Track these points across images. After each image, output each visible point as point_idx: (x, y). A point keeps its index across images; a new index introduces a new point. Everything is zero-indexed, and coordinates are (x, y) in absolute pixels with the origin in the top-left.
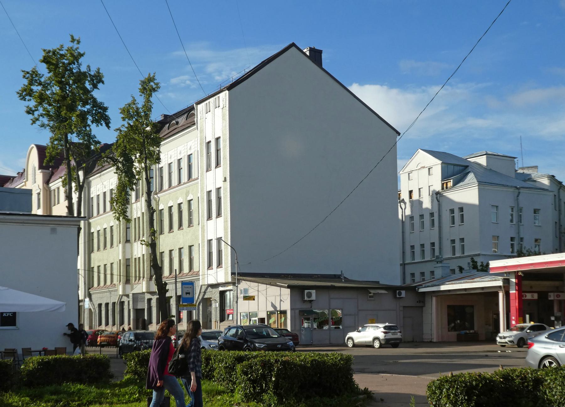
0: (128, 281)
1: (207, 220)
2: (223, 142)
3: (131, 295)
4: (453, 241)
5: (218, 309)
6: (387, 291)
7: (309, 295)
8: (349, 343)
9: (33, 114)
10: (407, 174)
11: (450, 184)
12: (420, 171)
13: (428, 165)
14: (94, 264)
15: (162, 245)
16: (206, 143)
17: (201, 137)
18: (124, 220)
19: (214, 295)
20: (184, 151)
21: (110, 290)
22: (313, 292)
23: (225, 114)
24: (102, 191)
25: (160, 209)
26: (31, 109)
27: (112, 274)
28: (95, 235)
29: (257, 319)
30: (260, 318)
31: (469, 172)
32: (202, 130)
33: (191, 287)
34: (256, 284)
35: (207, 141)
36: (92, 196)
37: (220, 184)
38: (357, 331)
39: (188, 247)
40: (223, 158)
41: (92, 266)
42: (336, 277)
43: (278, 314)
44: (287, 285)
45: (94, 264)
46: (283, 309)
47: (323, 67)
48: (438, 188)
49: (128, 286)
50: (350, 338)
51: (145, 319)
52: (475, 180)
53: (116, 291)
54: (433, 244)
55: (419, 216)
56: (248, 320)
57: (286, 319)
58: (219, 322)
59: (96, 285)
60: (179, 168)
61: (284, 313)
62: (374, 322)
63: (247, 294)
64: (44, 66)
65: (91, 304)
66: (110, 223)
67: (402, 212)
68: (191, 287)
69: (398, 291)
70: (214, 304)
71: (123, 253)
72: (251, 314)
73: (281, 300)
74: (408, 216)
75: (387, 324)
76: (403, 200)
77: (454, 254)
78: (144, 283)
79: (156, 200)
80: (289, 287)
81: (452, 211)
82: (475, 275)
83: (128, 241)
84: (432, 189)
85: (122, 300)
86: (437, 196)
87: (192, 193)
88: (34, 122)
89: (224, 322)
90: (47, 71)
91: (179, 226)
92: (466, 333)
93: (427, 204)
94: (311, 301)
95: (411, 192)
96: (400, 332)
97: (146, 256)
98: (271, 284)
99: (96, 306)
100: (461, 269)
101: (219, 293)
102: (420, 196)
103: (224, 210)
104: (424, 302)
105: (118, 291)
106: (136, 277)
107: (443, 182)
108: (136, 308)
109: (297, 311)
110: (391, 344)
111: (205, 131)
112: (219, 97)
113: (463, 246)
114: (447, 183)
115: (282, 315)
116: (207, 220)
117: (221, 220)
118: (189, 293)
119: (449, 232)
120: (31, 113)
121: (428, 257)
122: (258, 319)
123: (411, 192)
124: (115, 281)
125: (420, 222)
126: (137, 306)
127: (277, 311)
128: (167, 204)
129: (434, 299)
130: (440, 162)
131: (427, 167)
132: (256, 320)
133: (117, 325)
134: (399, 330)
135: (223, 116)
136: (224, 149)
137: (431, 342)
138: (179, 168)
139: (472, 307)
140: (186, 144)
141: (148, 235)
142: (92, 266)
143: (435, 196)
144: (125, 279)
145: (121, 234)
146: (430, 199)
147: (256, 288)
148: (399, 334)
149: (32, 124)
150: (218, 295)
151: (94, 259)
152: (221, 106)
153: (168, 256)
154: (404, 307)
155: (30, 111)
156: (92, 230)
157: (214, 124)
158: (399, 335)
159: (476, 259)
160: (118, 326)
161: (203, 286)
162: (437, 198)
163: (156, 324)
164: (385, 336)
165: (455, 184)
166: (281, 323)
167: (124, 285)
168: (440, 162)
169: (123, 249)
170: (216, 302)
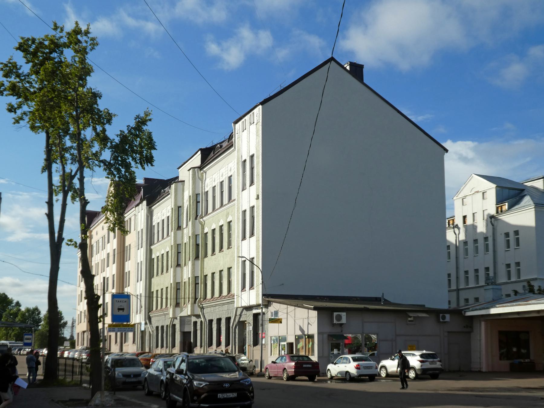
0: (177, 305)
1: (242, 240)
2: (256, 159)
3: (178, 318)
4: (508, 266)
5: (252, 332)
6: (429, 315)
7: (339, 318)
8: (382, 372)
9: (15, 112)
10: (461, 199)
11: (506, 207)
12: (474, 196)
13: (482, 189)
14: (154, 288)
15: (206, 268)
16: (242, 162)
17: (238, 156)
18: (120, 231)
19: (248, 317)
20: (225, 173)
21: (165, 313)
22: (344, 315)
23: (259, 130)
24: (161, 219)
25: (205, 232)
26: (12, 106)
27: (167, 298)
28: (155, 260)
29: (285, 343)
30: (289, 343)
31: (525, 195)
32: (239, 149)
33: (125, 302)
34: (286, 306)
35: (243, 160)
36: (153, 225)
37: (254, 202)
38: (390, 359)
39: (227, 269)
40: (257, 175)
41: (152, 291)
42: (377, 300)
43: (305, 338)
44: (313, 307)
45: (154, 289)
46: (310, 333)
47: (364, 81)
48: (493, 212)
49: (178, 309)
50: (384, 367)
51: (191, 342)
52: (531, 202)
53: (168, 314)
54: (487, 269)
55: (472, 241)
56: (278, 345)
57: (313, 345)
58: (252, 346)
59: (154, 308)
60: (221, 190)
61: (311, 337)
62: (414, 348)
63: (277, 317)
64: (21, 54)
65: (150, 327)
66: (166, 248)
67: (456, 237)
68: (125, 302)
69: (441, 315)
70: (248, 327)
71: (174, 278)
72: (280, 338)
73: (309, 324)
74: (461, 241)
75: (424, 352)
76: (457, 225)
77: (509, 279)
78: (189, 306)
79: (201, 224)
80: (315, 309)
81: (507, 235)
82: (531, 297)
83: (178, 265)
84: (486, 213)
85: (174, 323)
86: (492, 220)
87: (231, 215)
88: (17, 121)
89: (257, 347)
90: (25, 60)
91: (220, 249)
92: (520, 363)
93: (481, 228)
94: (341, 325)
95: (465, 217)
96: (440, 361)
97: (192, 279)
98: (299, 305)
99: (155, 328)
100: (516, 293)
101: (252, 315)
102: (474, 220)
103: (257, 229)
104: (471, 327)
105: (169, 315)
106: (146, 297)
107: (497, 206)
108: (183, 331)
109: (325, 336)
110: (430, 375)
111: (241, 150)
112: (253, 113)
113: (519, 271)
114: (501, 207)
115: (310, 340)
116: (242, 240)
117: (254, 239)
118: (123, 309)
119: (504, 257)
120: (12, 112)
121: (482, 282)
122: (287, 344)
123: (465, 217)
124: (169, 306)
125: (474, 247)
126: (184, 328)
127: (305, 335)
128: (211, 227)
129: (483, 324)
130: (494, 186)
131: (481, 192)
132: (285, 345)
133: (169, 347)
134: (439, 359)
135: (257, 132)
136: (257, 166)
137: (480, 372)
138: (221, 190)
139: (528, 333)
140: (227, 166)
141: (194, 259)
142: (152, 291)
143: (489, 220)
144: (175, 303)
145: (173, 259)
146: (485, 223)
147: (285, 311)
148: (438, 363)
149: (14, 123)
150: (252, 318)
151: (154, 284)
152: (255, 123)
153: (211, 279)
154: (449, 332)
155: (11, 109)
156: (153, 256)
157: (249, 142)
158: (438, 365)
159: (532, 283)
160: (171, 348)
161: (238, 309)
162: (491, 222)
163: (200, 347)
164: (421, 366)
165: (510, 207)
166: (309, 348)
167: (174, 308)
168: (494, 186)
169: (174, 273)
170: (250, 325)
